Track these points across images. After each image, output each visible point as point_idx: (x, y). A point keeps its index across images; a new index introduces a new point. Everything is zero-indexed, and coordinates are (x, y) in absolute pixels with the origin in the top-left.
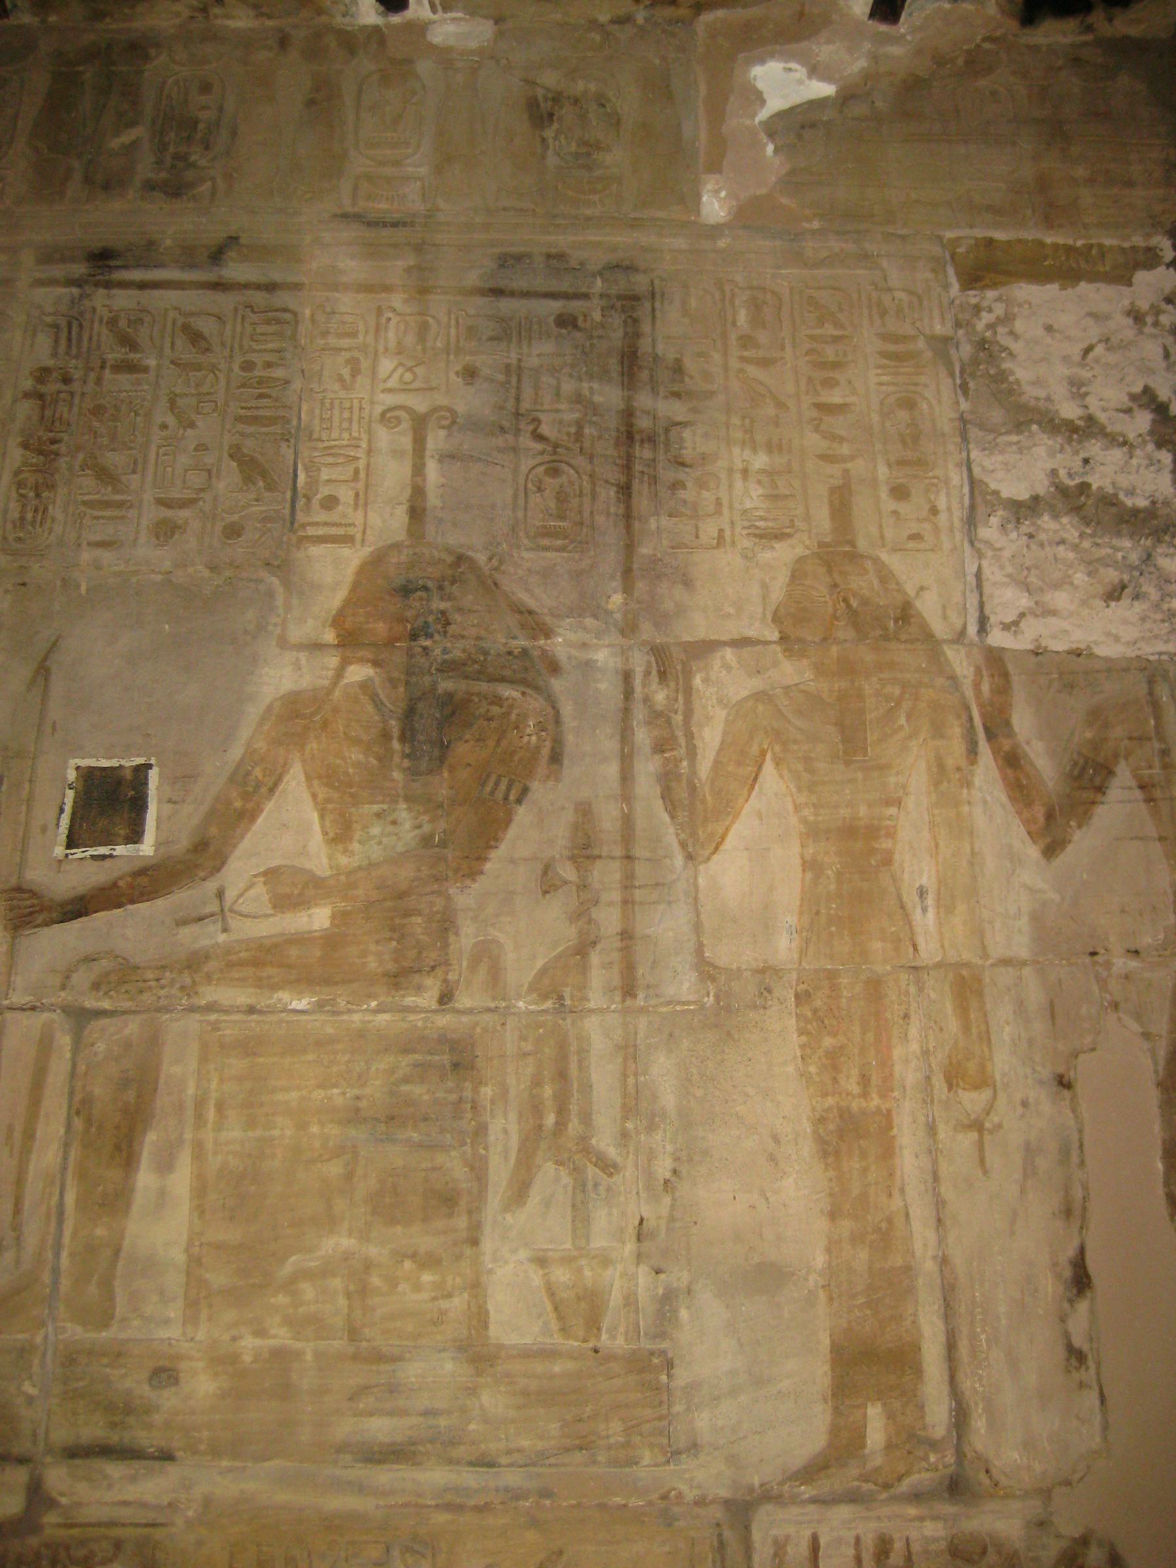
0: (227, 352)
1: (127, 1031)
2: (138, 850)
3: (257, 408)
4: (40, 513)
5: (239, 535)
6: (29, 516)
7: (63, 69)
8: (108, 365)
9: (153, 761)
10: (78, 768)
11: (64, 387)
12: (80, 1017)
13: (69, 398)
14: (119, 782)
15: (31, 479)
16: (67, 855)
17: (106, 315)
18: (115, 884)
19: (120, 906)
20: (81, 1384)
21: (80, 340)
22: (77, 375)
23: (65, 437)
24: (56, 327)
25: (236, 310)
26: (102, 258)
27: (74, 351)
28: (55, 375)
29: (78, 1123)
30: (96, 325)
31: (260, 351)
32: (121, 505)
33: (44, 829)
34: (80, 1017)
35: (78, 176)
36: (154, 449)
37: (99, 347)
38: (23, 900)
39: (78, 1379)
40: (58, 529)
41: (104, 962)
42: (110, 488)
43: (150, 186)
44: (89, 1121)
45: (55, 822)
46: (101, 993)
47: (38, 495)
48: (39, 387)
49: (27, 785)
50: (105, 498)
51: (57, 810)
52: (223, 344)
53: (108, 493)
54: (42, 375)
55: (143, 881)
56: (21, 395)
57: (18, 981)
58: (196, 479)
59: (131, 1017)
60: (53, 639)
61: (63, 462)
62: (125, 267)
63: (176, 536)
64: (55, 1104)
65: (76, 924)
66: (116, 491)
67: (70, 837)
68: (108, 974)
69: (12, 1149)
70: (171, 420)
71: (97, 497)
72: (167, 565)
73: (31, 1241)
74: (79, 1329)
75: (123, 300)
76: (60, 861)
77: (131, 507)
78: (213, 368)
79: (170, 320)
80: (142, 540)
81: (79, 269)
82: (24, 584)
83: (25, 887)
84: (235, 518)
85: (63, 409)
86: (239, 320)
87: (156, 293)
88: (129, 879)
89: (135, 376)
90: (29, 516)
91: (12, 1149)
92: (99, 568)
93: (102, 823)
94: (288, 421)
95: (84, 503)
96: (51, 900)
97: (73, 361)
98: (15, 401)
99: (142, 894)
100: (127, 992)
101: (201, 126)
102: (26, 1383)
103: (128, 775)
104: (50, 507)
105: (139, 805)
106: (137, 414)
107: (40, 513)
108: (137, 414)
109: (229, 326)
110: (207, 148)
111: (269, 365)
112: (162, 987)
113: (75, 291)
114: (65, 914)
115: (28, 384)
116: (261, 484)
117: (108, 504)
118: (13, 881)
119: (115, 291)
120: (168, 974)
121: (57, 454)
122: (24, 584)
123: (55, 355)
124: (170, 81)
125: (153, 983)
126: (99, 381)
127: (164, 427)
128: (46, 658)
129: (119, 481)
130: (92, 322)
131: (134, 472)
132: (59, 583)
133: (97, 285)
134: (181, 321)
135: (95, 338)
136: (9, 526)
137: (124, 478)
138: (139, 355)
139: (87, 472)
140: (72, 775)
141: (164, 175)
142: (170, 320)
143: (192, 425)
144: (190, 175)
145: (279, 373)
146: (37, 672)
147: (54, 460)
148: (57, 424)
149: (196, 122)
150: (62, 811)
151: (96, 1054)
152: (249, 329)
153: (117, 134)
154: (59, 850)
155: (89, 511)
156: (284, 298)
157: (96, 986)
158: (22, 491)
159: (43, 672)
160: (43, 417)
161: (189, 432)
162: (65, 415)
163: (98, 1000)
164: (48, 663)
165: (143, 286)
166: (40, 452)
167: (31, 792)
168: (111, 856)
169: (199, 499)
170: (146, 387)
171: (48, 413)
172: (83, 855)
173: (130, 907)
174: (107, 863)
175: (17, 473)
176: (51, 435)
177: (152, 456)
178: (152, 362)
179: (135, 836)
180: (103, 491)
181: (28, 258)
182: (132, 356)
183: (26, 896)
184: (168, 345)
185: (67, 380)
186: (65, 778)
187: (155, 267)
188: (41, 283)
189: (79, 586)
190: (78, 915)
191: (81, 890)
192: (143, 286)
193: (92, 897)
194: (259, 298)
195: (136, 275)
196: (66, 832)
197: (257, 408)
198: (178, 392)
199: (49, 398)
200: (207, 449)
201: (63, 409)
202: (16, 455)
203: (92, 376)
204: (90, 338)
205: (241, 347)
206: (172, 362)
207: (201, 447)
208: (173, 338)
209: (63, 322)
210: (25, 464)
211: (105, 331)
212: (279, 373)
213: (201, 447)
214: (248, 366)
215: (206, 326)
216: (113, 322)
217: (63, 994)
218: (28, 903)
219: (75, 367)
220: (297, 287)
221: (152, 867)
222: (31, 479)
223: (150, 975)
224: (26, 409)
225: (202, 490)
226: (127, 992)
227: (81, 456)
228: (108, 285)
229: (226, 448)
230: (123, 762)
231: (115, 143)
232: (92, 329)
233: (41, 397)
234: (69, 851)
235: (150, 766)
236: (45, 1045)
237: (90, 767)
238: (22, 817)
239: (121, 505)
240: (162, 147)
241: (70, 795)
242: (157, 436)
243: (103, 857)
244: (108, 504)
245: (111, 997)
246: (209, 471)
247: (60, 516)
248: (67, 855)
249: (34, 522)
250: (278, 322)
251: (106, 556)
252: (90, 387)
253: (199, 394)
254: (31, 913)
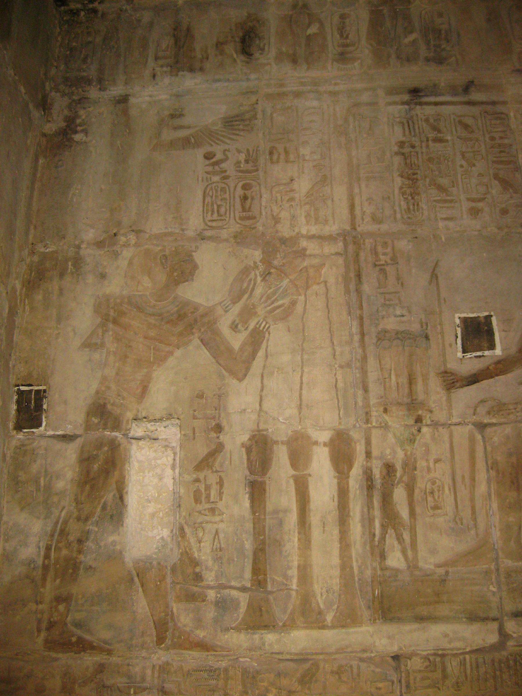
0: (481, 133)
1: (506, 432)
2: (494, 353)
3: (500, 157)
4: (416, 206)
5: (507, 214)
6: (411, 207)
7: (373, 9)
8: (430, 139)
9: (492, 313)
10: (459, 318)
11: (413, 150)
12: (482, 427)
13: (416, 154)
14: (479, 324)
15: (408, 191)
16: (463, 356)
17: (423, 118)
18: (488, 368)
19: (492, 377)
20: (515, 585)
21: (414, 129)
22: (417, 144)
23: (419, 172)
24: (403, 123)
25: (481, 114)
26: (415, 92)
27: (413, 134)
28: (406, 144)
29: (493, 473)
30: (420, 122)
31: (496, 132)
32: (451, 201)
33: (451, 345)
34: (482, 427)
35: (394, 56)
36: (459, 176)
37: (423, 132)
38: (448, 377)
39: (513, 583)
40: (426, 213)
41: (490, 402)
42: (444, 194)
43: (427, 60)
44: (497, 471)
45: (455, 342)
46: (491, 416)
47: (413, 198)
48: (401, 150)
49: (439, 327)
50: (443, 198)
51: (455, 337)
52: (478, 129)
53: (443, 196)
54: (401, 144)
55: (500, 366)
56: (393, 154)
57: (454, 412)
58: (482, 189)
59: (506, 426)
60: (435, 262)
61: (420, 183)
62: (426, 96)
63: (480, 214)
64: (481, 465)
65: (474, 386)
66: (447, 195)
67: (463, 348)
68: (493, 407)
69: (465, 485)
70: (464, 163)
71: (439, 198)
72: (478, 227)
73: (482, 526)
74: (510, 562)
75: (429, 110)
76: (461, 359)
77: (456, 202)
78: (477, 140)
79: (452, 119)
80: (465, 216)
81: (406, 97)
82: (416, 238)
83: (448, 371)
84: (504, 206)
85: (414, 159)
86: (483, 118)
87: (443, 107)
88: (494, 366)
89: (443, 144)
90: (411, 207)
91: (465, 485)
92: (448, 229)
93: (476, 341)
94: (515, 163)
95: (435, 201)
96: (462, 376)
97: (414, 138)
98: (392, 157)
99: (500, 372)
100: (502, 415)
101: (443, 32)
102: (491, 586)
103: (483, 320)
104: (420, 203)
105: (490, 333)
106: (448, 161)
107: (416, 206)
108: (448, 161)
109: (479, 121)
110: (448, 42)
111: (501, 138)
112: (518, 412)
113: (407, 107)
114: (469, 382)
115: (396, 149)
116: (511, 190)
117: (445, 201)
118: (442, 369)
119: (424, 107)
120: (519, 406)
121: (417, 179)
122: (416, 238)
123: (404, 135)
124: (423, 12)
125: (513, 411)
126: (427, 146)
127: (462, 166)
128: (434, 270)
129: (448, 191)
130: (418, 121)
131: (453, 186)
132: (432, 237)
133: (416, 104)
134: (457, 119)
135: (421, 127)
136: (403, 212)
137: (449, 189)
138: (442, 135)
139: (432, 187)
140: (458, 321)
141: (432, 54)
142: (452, 119)
143: (474, 165)
144: (444, 54)
145: (506, 141)
146: (432, 277)
147: (416, 182)
148: (413, 166)
149: (440, 31)
150: (457, 337)
151: (494, 442)
152: (488, 123)
153: (406, 37)
154: (460, 355)
155: (437, 204)
156: (499, 108)
157: (489, 413)
158: (405, 196)
159: (434, 276)
160: (406, 163)
161: (473, 168)
162: (416, 162)
163: (490, 419)
164: (435, 272)
165: (436, 104)
166: (409, 179)
167: (442, 329)
168: (483, 356)
169: (485, 198)
170: (449, 149)
171: (408, 161)
172: (471, 356)
173: (497, 378)
174: (482, 359)
175: (401, 188)
176: (412, 171)
177: (460, 180)
178: (449, 138)
179: (492, 347)
180: (441, 195)
181: (381, 93)
182: (439, 135)
183: (449, 375)
184: (454, 130)
185: (413, 147)
186: (455, 323)
187: (439, 95)
188: (390, 104)
189: (441, 238)
190: (474, 382)
191: (473, 372)
192: (436, 104)
193: (479, 374)
194: (489, 108)
195: (432, 99)
196: (461, 346)
197: (500, 157)
198: (464, 150)
199: (407, 155)
200: (483, 176)
201: (414, 159)
202: (399, 181)
203: (424, 145)
204: (419, 128)
205: (487, 131)
206: (458, 137)
207: (480, 175)
208: (456, 128)
209: (405, 121)
210: (403, 184)
211: (424, 124)
212: (506, 141)
213: (480, 175)
214: (492, 139)
215: (470, 121)
216: (427, 120)
217: (474, 417)
218: (452, 378)
219: (416, 141)
220: (504, 103)
221: (502, 360)
222: (408, 191)
223: (511, 407)
224: (397, 160)
225: (485, 194)
226: (502, 415)
227: (428, 180)
228: (421, 104)
229: (492, 175)
230: (479, 315)
231: (406, 41)
232: (418, 124)
233: (403, 154)
234: (464, 355)
235: (491, 316)
236: (472, 440)
237: (465, 317)
238: (440, 341)
239: (451, 201)
240: (428, 43)
241: (459, 330)
242: (459, 170)
243: (480, 357)
244: (445, 201)
245: (496, 417)
246: (487, 186)
247: (425, 207)
248: (463, 356)
249: (414, 210)
250: (500, 119)
251: (451, 224)
252: (424, 150)
253: (474, 152)
254: (453, 382)
